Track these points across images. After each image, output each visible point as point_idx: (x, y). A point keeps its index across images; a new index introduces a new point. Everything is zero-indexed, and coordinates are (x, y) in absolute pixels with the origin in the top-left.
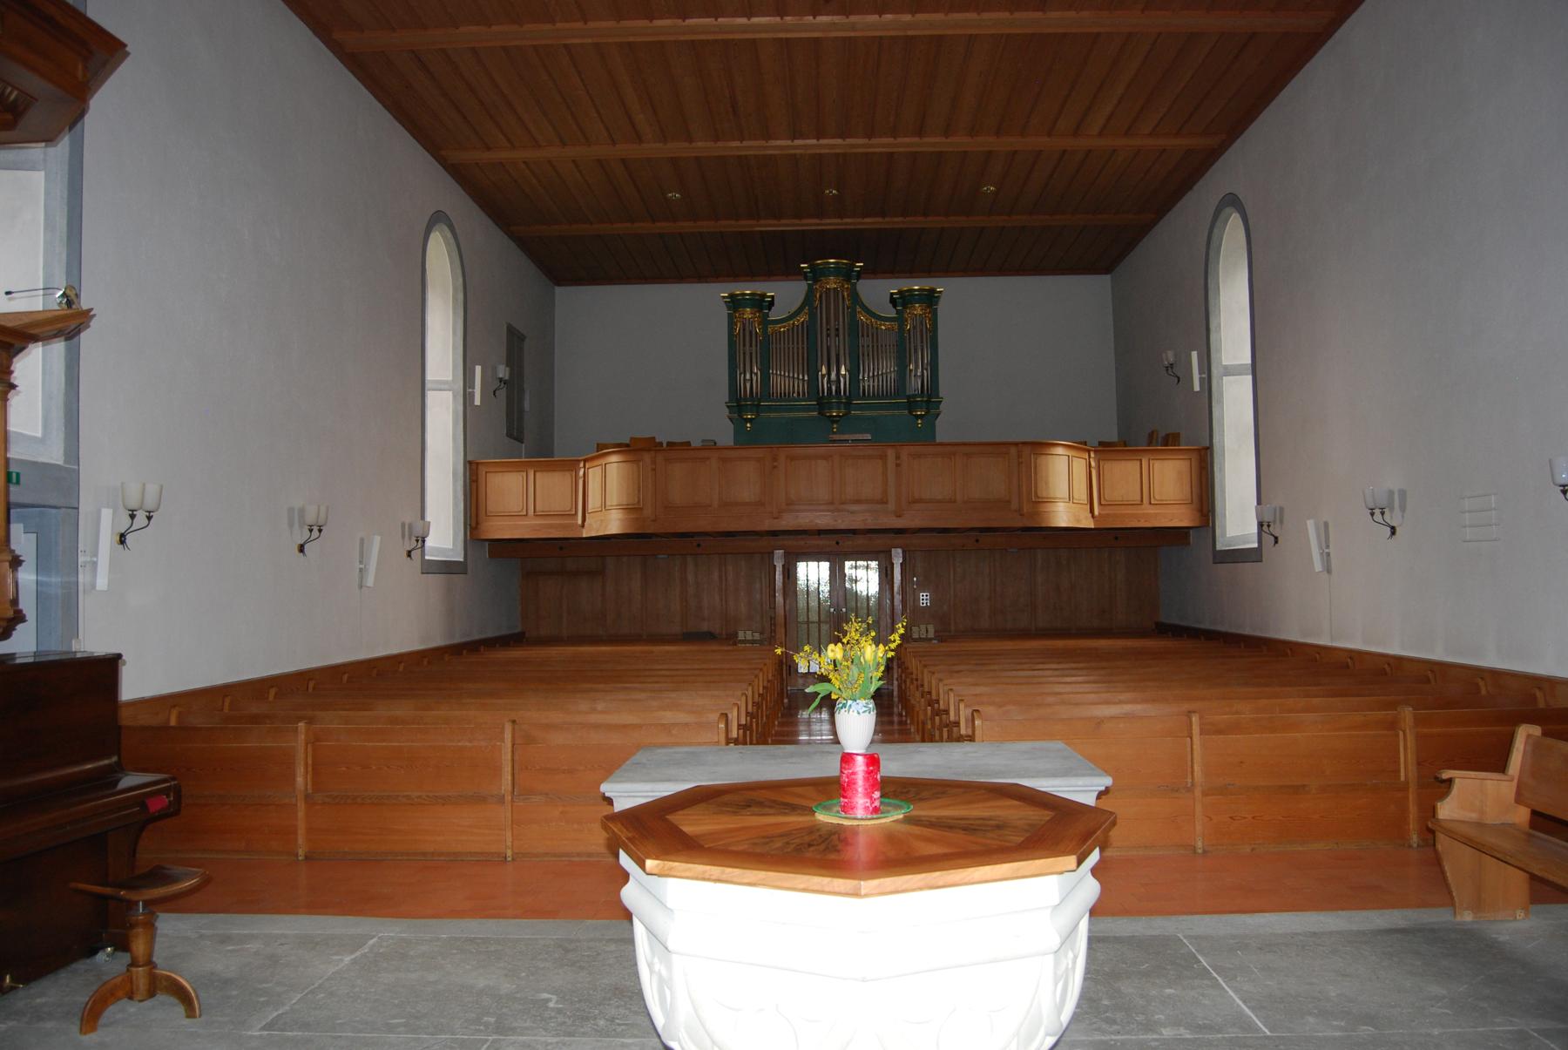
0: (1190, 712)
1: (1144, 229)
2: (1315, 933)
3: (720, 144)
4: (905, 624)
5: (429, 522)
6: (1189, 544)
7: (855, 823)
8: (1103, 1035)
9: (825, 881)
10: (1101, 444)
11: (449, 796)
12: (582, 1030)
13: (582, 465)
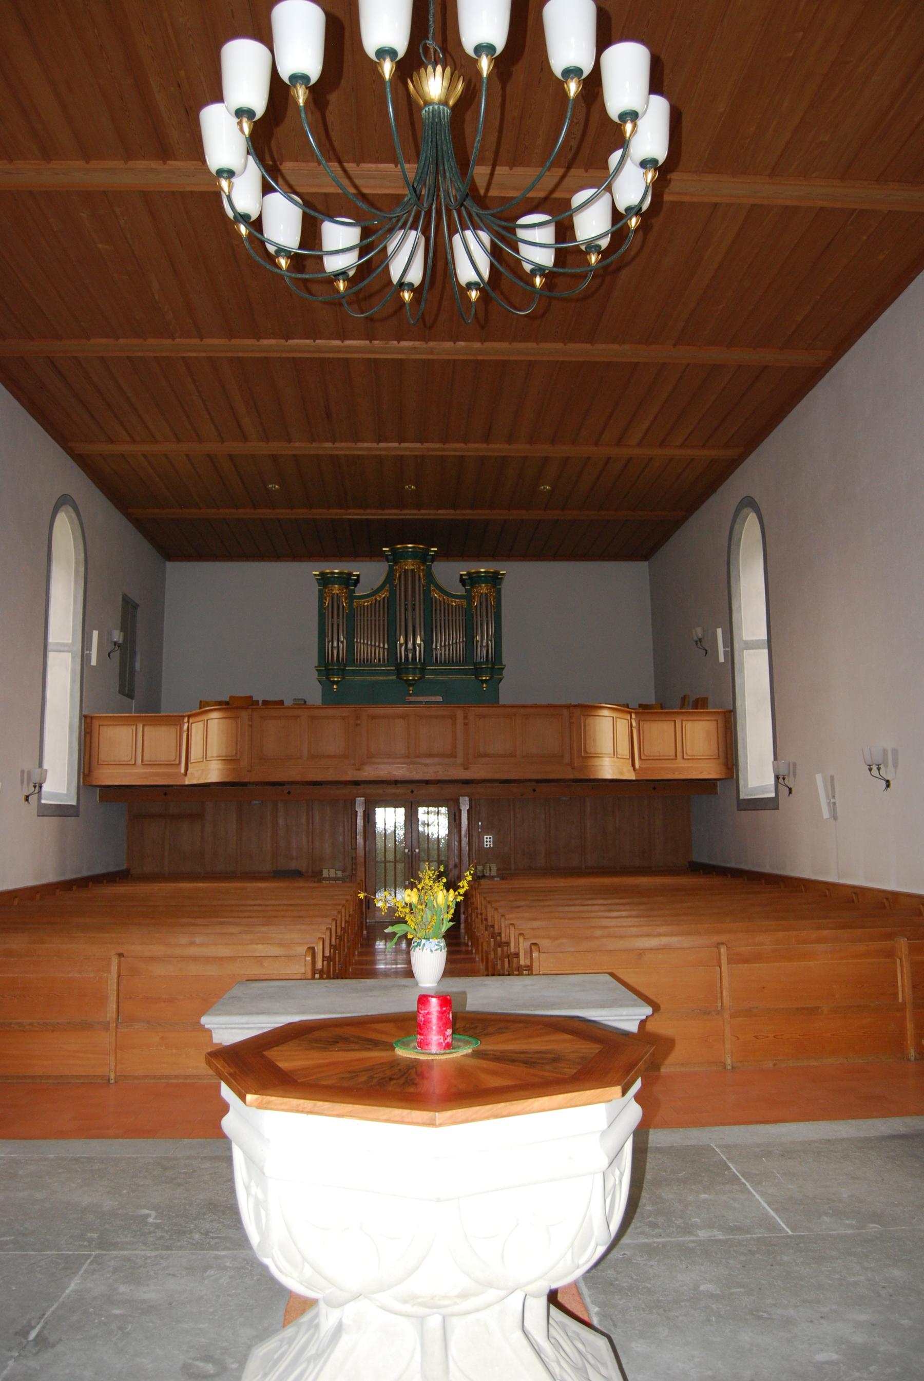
0: (719, 944)
1: (677, 524)
2: (829, 1141)
3: (314, 445)
4: (472, 872)
5: (47, 770)
6: (716, 793)
7: (430, 1058)
8: (647, 1238)
9: (405, 1113)
10: (640, 706)
11: (58, 1023)
12: (179, 1244)
13: (186, 720)
